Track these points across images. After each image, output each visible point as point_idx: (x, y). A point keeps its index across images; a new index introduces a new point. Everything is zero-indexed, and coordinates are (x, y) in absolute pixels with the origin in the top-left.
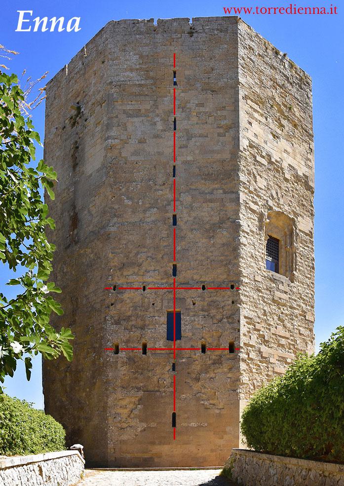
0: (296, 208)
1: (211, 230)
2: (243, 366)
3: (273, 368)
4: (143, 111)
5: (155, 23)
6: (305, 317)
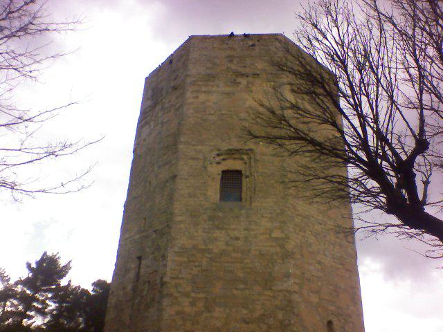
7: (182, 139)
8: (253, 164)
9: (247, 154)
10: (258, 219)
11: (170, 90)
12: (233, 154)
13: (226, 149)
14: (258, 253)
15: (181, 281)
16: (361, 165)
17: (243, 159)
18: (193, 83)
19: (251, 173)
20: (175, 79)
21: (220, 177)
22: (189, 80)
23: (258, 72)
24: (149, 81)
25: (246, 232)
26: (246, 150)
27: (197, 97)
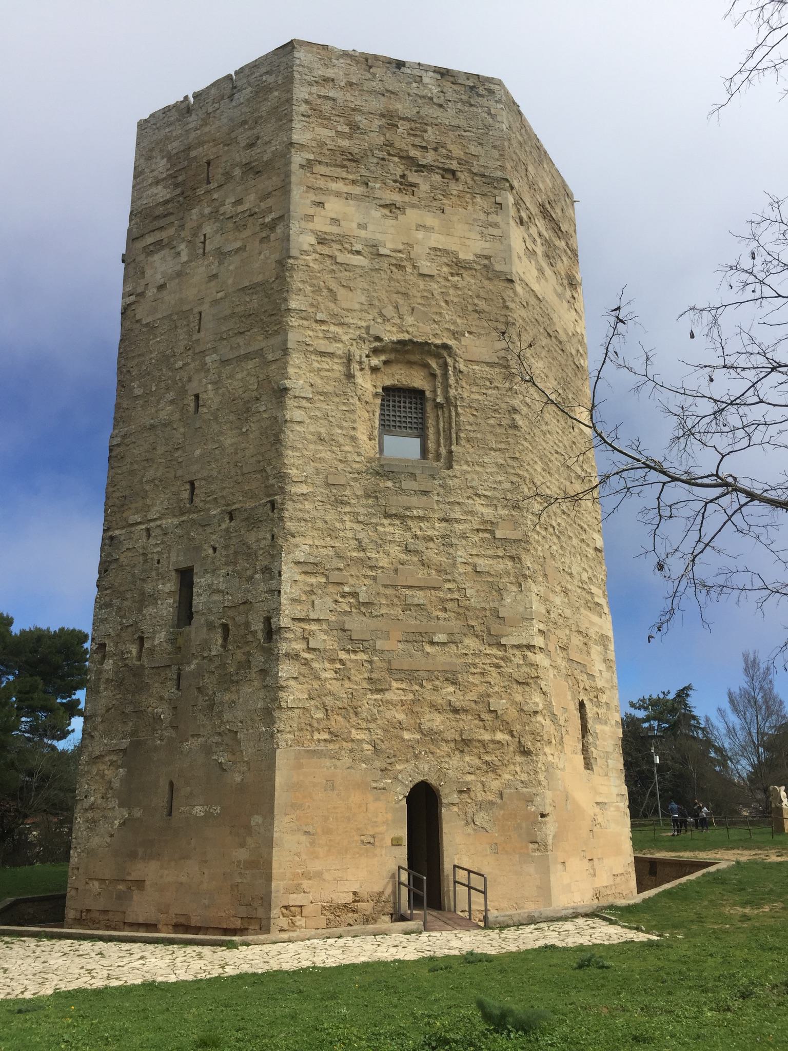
0: (454, 323)
1: (243, 411)
2: (286, 670)
3: (389, 662)
4: (166, 241)
5: (192, 100)
6: (492, 532)
7: (293, 305)
8: (452, 381)
9: (438, 356)
10: (468, 498)
11: (237, 172)
12: (407, 352)
13: (395, 339)
14: (469, 569)
15: (314, 627)
16: (100, 932)
17: (427, 366)
18: (308, 165)
19: (447, 398)
20: (251, 145)
21: (379, 401)
22: (298, 158)
23: (454, 165)
24: (142, 126)
25: (444, 524)
26: (436, 346)
27: (321, 204)
